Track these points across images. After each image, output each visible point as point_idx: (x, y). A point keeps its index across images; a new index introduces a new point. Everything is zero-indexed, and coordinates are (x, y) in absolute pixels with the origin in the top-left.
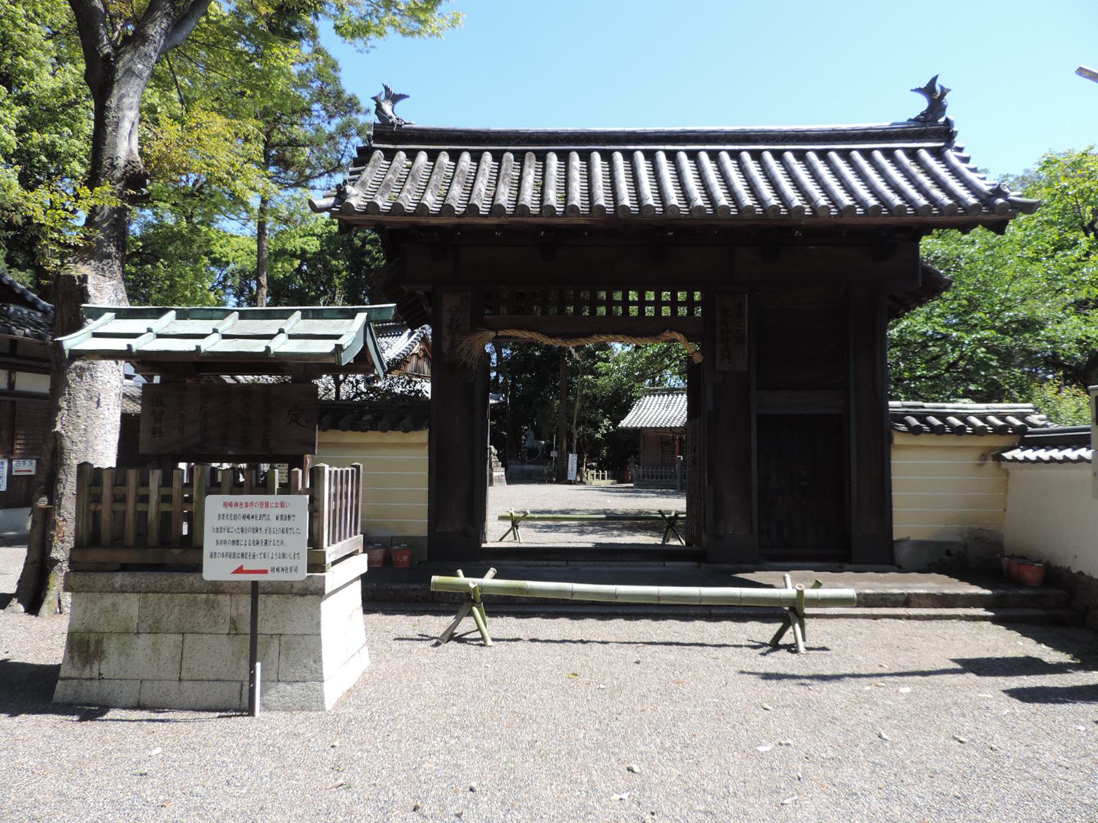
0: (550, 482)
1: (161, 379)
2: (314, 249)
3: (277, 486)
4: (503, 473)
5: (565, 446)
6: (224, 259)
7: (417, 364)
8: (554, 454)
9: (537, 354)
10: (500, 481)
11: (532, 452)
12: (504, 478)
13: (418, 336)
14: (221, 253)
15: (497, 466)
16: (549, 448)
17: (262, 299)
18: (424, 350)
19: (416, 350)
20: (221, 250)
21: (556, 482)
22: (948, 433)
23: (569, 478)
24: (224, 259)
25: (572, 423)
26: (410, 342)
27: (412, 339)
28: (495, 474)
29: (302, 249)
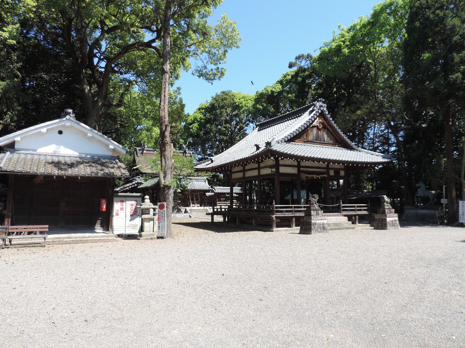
0: (442, 224)
1: (345, 173)
2: (278, 90)
3: (237, 220)
4: (397, 219)
5: (454, 194)
6: (240, 105)
7: (317, 134)
8: (444, 201)
9: (424, 126)
10: (393, 224)
11: (425, 200)
12: (398, 222)
13: (316, 112)
14: (239, 102)
15: (391, 212)
16: (439, 196)
17: (165, 82)
18: (323, 124)
19: (315, 123)
20: (239, 101)
21: (448, 224)
22: (159, 178)
23: (461, 221)
24: (240, 105)
25: (460, 176)
26: (310, 117)
27: (312, 115)
28: (388, 219)
29: (272, 91)
